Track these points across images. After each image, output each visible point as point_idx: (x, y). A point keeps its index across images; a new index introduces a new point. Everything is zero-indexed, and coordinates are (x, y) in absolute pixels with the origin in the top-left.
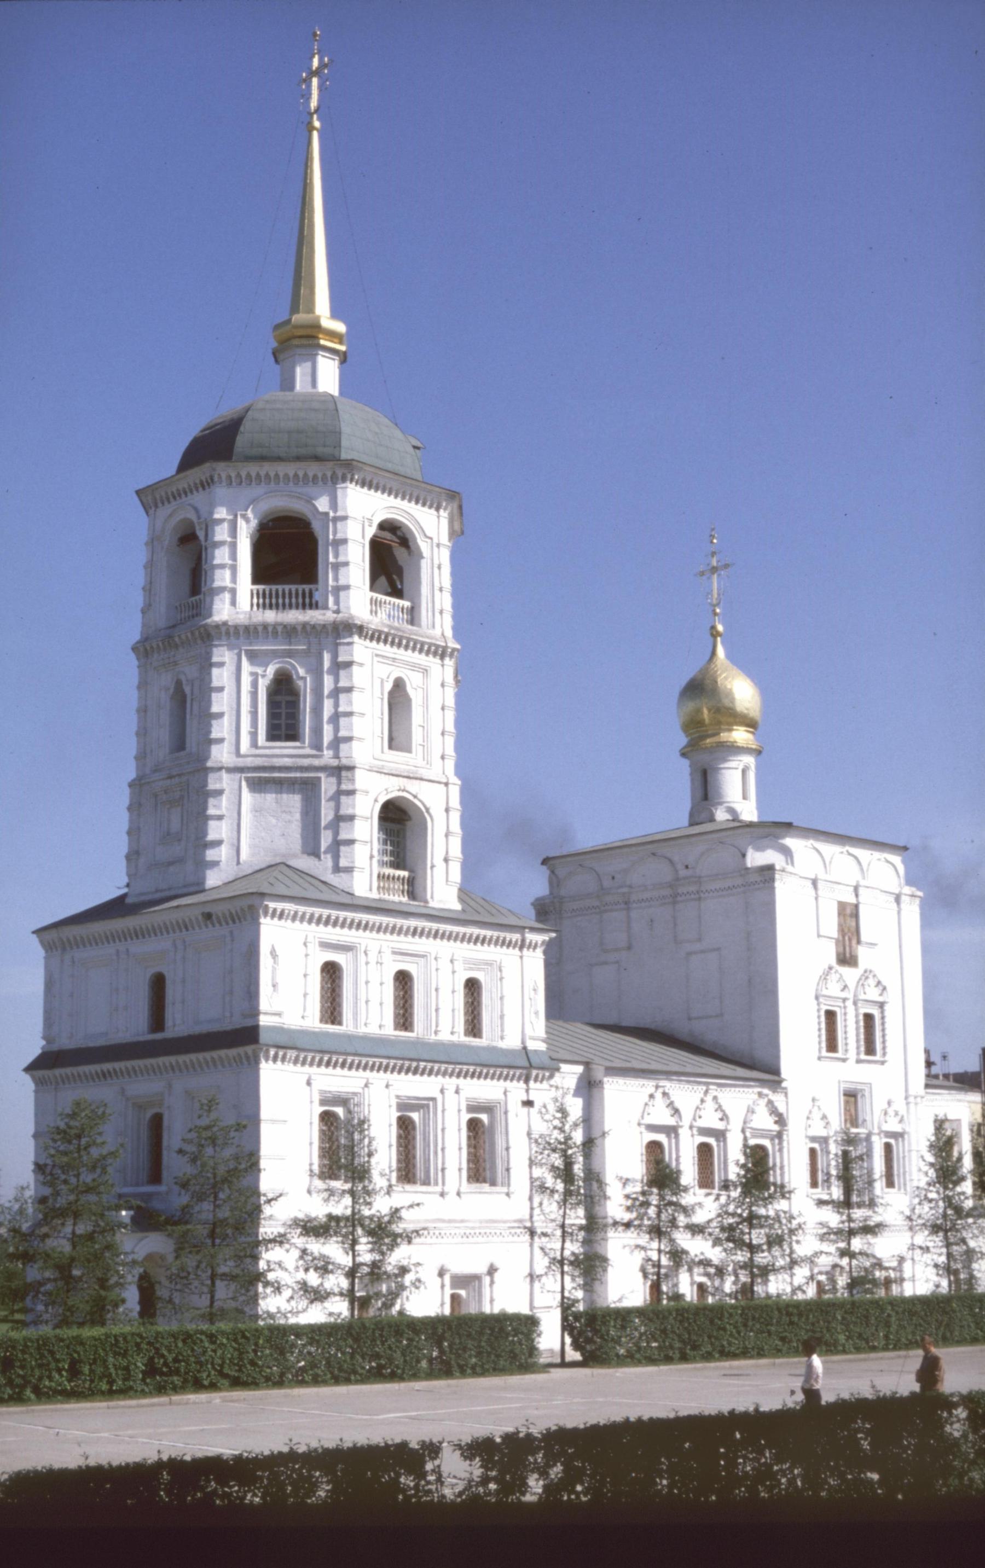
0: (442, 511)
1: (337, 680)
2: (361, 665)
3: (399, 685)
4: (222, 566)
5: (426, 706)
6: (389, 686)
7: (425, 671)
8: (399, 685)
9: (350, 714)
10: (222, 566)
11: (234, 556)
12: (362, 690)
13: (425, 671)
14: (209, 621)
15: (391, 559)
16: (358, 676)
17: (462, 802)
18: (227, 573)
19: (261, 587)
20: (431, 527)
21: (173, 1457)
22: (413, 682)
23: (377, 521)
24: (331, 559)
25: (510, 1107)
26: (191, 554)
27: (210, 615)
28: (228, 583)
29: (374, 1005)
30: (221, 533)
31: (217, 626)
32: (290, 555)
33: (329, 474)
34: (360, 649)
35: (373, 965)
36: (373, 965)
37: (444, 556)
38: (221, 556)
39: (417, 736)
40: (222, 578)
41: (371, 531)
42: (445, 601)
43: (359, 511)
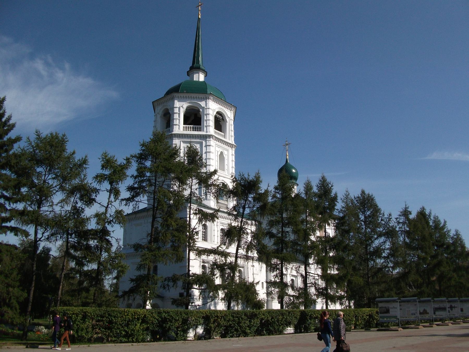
0: (233, 149)
1: (206, 143)
2: (213, 159)
3: (222, 153)
4: (176, 125)
5: (228, 160)
6: (219, 153)
7: (228, 151)
8: (222, 153)
9: (210, 146)
10: (176, 125)
11: (179, 117)
12: (213, 153)
13: (228, 151)
14: (173, 133)
15: (219, 123)
16: (212, 149)
17: (235, 159)
18: (178, 121)
19: (186, 126)
20: (229, 114)
21: (45, 133)
22: (225, 153)
23: (216, 111)
24: (205, 119)
25: (249, 267)
26: (168, 118)
27: (173, 131)
28: (178, 123)
29: (216, 237)
30: (176, 110)
31: (175, 134)
32: (194, 118)
33: (205, 97)
34: (212, 142)
35: (215, 226)
36: (215, 226)
37: (232, 122)
38: (176, 116)
39: (226, 167)
40: (176, 122)
41: (215, 113)
42: (232, 133)
43: (212, 107)
